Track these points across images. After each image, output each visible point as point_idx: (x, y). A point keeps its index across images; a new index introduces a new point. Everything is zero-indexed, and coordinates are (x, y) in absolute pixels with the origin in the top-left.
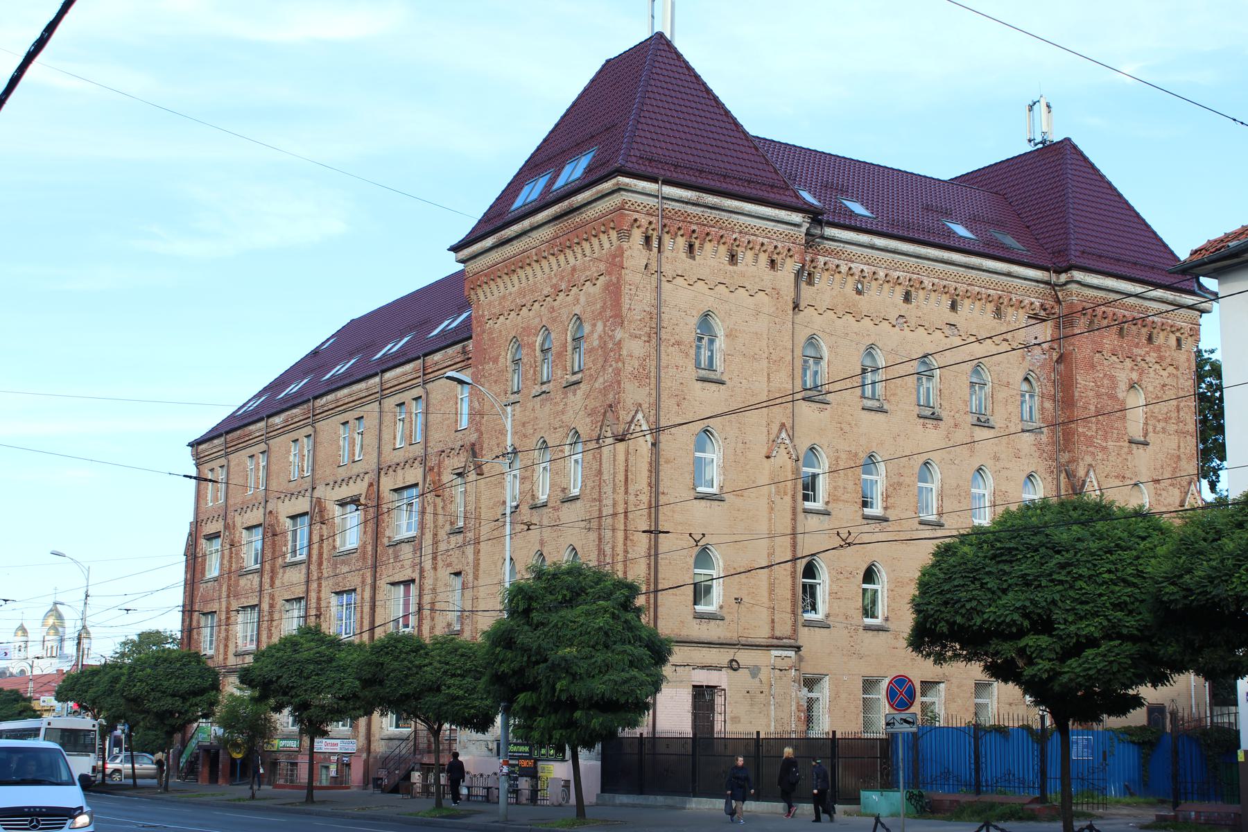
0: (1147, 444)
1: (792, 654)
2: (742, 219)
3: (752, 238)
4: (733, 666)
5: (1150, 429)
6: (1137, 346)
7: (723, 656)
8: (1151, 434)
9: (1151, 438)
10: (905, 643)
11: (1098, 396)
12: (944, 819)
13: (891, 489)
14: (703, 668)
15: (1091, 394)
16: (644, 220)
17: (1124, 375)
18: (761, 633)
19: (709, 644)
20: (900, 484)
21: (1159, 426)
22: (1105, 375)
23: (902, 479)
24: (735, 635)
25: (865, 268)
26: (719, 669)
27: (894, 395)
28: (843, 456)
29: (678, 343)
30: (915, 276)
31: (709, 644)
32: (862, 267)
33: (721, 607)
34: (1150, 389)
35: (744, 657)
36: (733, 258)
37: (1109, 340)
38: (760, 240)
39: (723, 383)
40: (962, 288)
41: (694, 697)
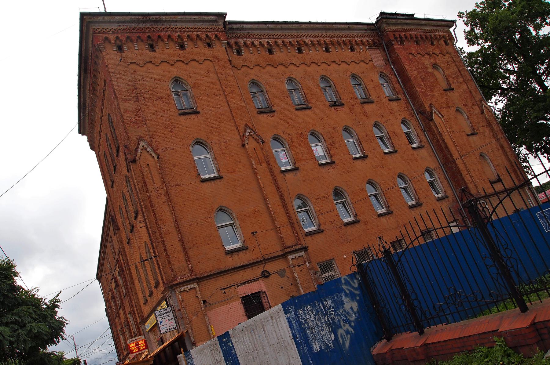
0: (453, 89)
1: (303, 254)
2: (179, 25)
3: (189, 33)
4: (265, 275)
5: (451, 83)
6: (427, 47)
7: (257, 271)
8: (452, 85)
9: (453, 86)
10: (66, 328)
11: (419, 73)
12: (275, 161)
13: (329, 146)
14: (244, 283)
15: (416, 73)
16: (112, 38)
17: (427, 62)
18: (275, 249)
19: (244, 267)
20: (334, 142)
21: (455, 81)
22: (418, 63)
23: (334, 140)
24: (260, 255)
25: (269, 40)
26: (257, 280)
27: (312, 99)
28: (294, 136)
29: (160, 98)
30: (299, 39)
31: (244, 267)
32: (267, 40)
33: (244, 242)
34: (442, 65)
35: (271, 267)
36: (182, 47)
37: (413, 48)
38: (195, 33)
39: (198, 113)
40: (328, 40)
41: (245, 305)
